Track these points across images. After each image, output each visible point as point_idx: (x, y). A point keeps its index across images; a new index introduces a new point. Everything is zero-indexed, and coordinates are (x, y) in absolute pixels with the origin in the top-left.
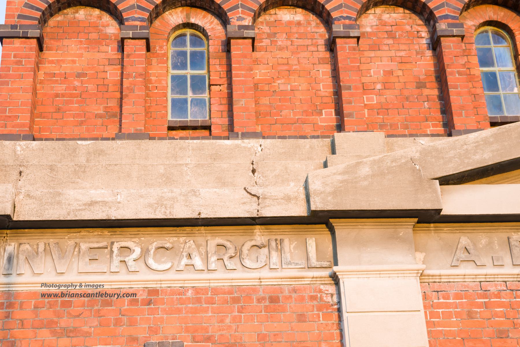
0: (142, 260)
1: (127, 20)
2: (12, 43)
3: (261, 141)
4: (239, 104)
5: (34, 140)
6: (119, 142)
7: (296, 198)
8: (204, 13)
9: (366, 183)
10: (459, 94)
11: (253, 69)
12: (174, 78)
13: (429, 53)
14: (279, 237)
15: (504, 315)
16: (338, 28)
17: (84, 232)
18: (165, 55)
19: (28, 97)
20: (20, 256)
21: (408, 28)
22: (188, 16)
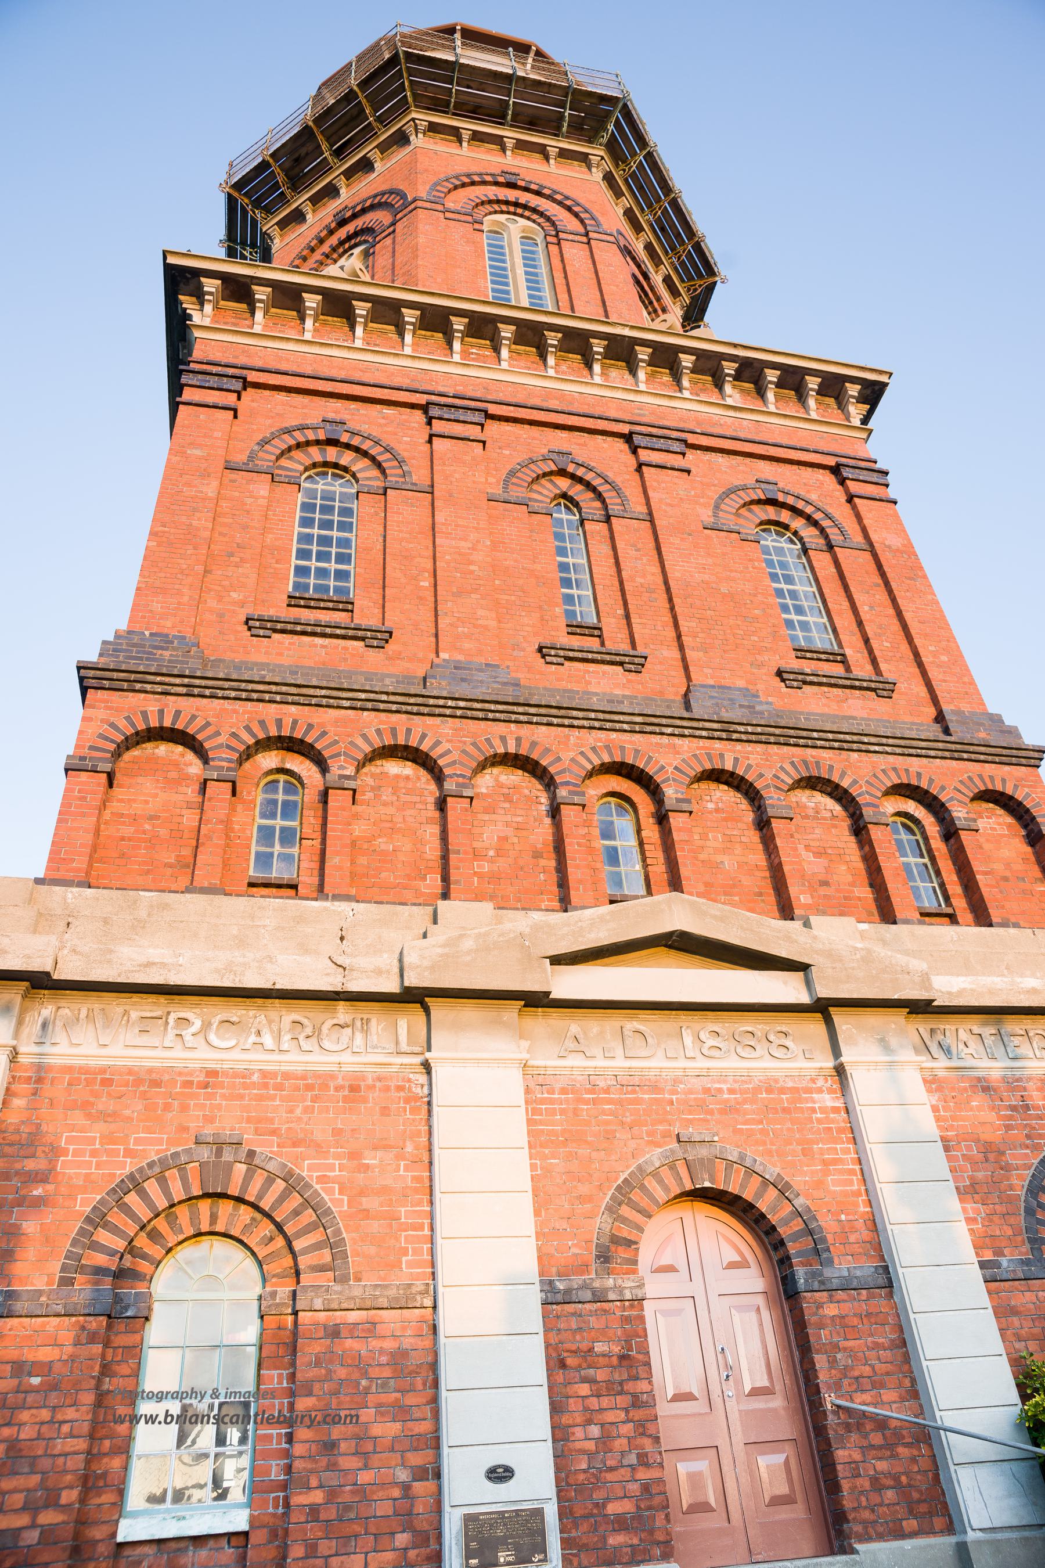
0: (202, 1035)
1: (213, 759)
2: (78, 777)
3: (354, 905)
4: (333, 861)
5: (90, 887)
6: (188, 896)
7: (388, 972)
8: (302, 758)
9: (469, 958)
10: (578, 867)
11: (349, 823)
12: (261, 828)
13: (548, 821)
14: (365, 1016)
16: (449, 785)
17: (136, 998)
18: (254, 801)
19: (89, 838)
20: (57, 1022)
21: (526, 792)
22: (283, 761)
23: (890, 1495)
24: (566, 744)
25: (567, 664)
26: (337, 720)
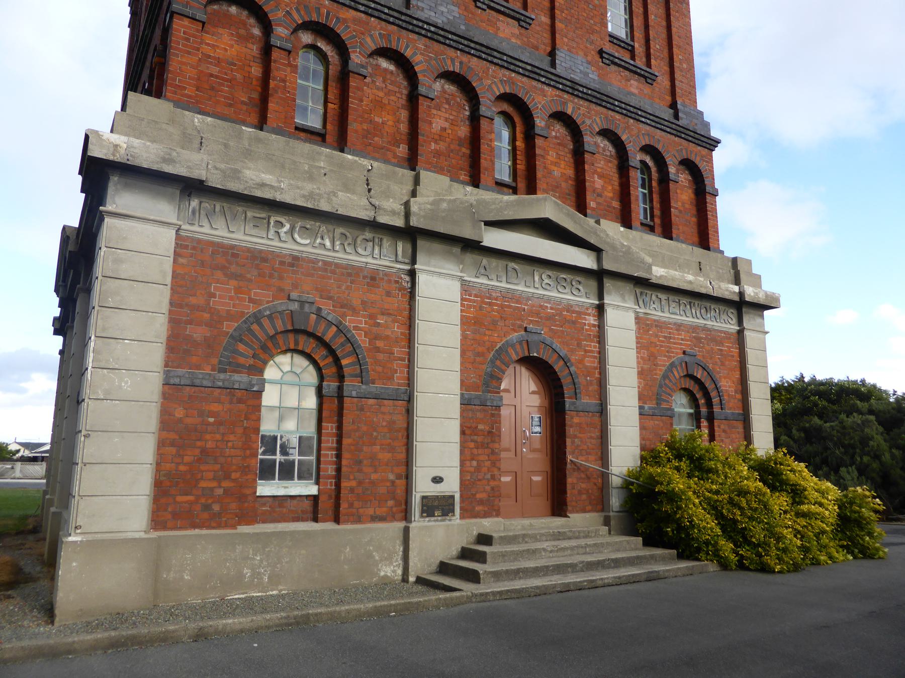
7: (399, 214)
10: (485, 159)
15: (497, 311)
21: (458, 99)
23: (584, 497)
24: (487, 74)
25: (488, 10)
26: (354, 20)
